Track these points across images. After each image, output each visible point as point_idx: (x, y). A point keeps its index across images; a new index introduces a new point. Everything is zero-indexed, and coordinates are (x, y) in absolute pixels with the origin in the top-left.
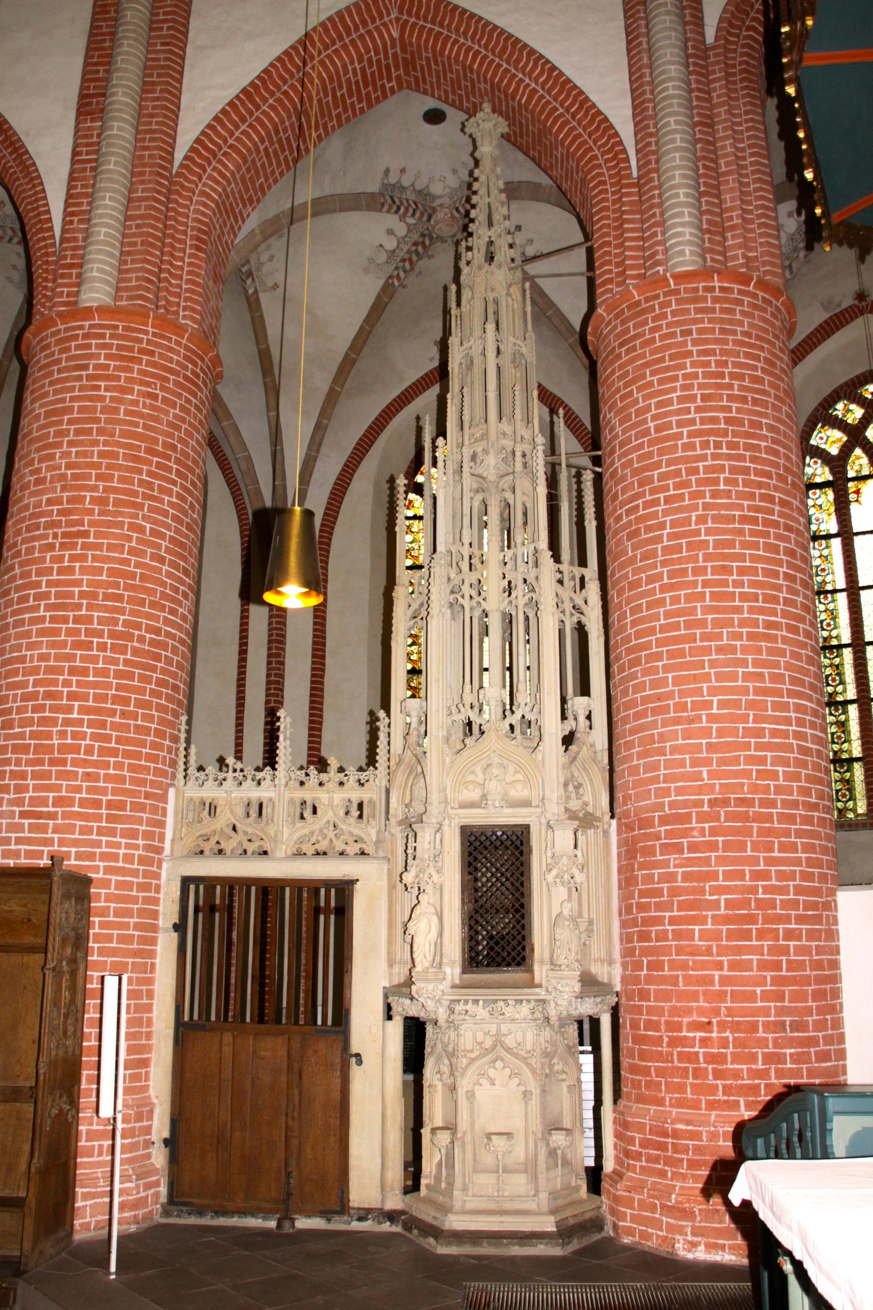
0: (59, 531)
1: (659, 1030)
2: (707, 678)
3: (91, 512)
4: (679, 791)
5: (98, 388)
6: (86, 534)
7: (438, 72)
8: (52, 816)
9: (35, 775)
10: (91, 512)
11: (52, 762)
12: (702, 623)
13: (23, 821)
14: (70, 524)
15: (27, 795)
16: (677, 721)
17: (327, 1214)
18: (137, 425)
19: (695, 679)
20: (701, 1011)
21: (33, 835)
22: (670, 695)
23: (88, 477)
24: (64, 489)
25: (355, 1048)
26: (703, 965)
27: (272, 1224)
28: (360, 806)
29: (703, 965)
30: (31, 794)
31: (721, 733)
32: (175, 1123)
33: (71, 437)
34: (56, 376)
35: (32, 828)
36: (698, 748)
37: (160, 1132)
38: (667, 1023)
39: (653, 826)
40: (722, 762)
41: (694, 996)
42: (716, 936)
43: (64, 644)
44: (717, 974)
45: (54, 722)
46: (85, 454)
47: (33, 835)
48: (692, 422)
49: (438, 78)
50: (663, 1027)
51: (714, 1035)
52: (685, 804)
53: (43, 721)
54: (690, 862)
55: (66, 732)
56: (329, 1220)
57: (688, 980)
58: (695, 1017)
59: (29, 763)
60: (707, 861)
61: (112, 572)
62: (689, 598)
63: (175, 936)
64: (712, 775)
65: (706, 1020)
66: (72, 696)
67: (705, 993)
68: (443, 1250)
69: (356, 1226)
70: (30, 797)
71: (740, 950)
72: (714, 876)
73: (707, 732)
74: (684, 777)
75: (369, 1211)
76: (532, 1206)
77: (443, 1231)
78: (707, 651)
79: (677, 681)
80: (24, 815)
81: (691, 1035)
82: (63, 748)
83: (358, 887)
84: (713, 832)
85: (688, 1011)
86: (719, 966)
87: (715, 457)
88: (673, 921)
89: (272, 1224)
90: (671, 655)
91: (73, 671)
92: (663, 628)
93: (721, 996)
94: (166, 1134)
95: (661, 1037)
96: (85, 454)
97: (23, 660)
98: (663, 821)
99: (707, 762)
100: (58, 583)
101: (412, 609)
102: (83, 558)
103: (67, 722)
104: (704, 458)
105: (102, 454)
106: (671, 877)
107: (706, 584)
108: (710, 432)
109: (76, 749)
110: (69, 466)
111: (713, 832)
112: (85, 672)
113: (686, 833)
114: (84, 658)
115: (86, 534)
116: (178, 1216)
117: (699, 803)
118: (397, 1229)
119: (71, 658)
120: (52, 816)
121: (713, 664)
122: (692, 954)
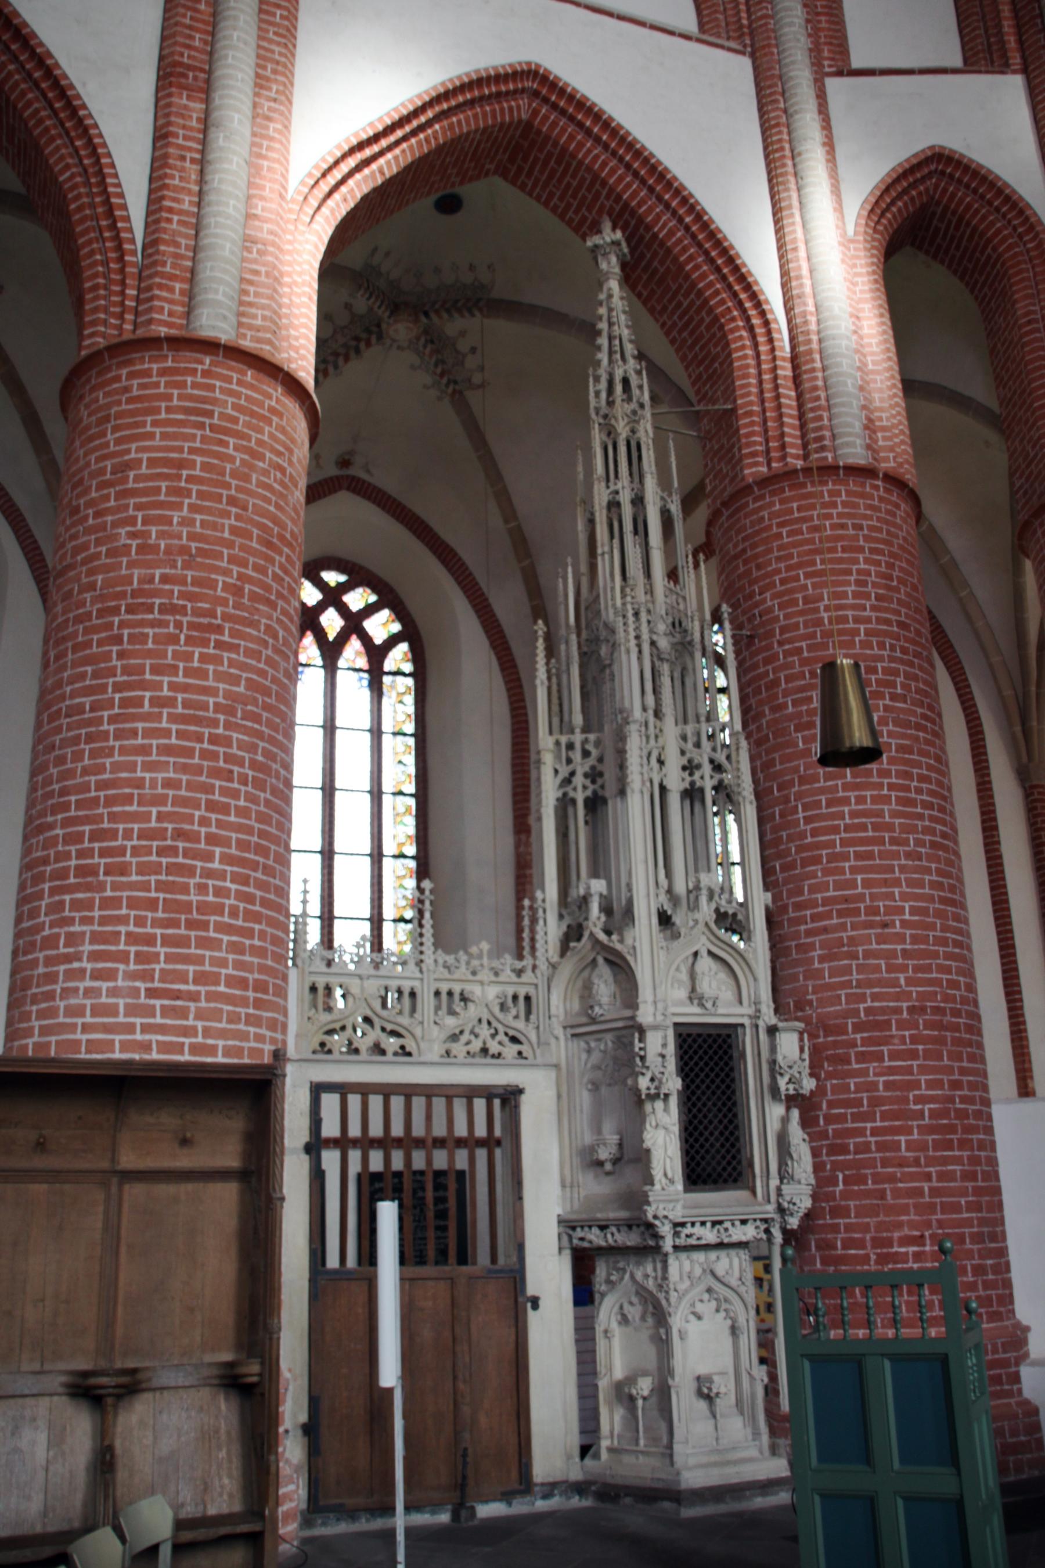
0: (185, 620)
1: (864, 1247)
2: (897, 883)
3: (224, 602)
4: (875, 997)
5: (225, 444)
6: (219, 629)
7: (553, 171)
8: (194, 997)
9: (167, 941)
10: (224, 602)
11: (191, 925)
12: (890, 828)
13: (152, 1002)
14: (196, 612)
15: (157, 967)
16: (870, 925)
17: (507, 1497)
18: (268, 501)
19: (885, 883)
20: (912, 1225)
21: (169, 1022)
22: (861, 898)
23: (219, 556)
24: (187, 566)
25: (531, 1290)
26: (912, 1177)
27: (444, 1518)
28: (528, 998)
29: (912, 1177)
30: (162, 965)
31: (915, 939)
32: (314, 1402)
33: (193, 500)
34: (163, 415)
35: (166, 1011)
36: (893, 954)
37: (294, 1415)
38: (873, 1239)
39: (846, 1033)
40: (917, 969)
41: (904, 1210)
42: (922, 1147)
43: (198, 770)
44: (926, 1186)
45: (191, 871)
46: (214, 526)
47: (169, 1022)
48: (868, 620)
49: (551, 177)
50: (869, 1244)
51: (928, 1248)
52: (883, 1010)
53: (174, 869)
54: (892, 1071)
55: (206, 886)
56: (510, 1504)
57: (897, 1193)
58: (906, 1231)
59: (156, 923)
60: (909, 1070)
61: (251, 684)
62: (875, 800)
63: (305, 1158)
64: (909, 981)
65: (917, 1233)
66: (211, 839)
67: (915, 1206)
68: (688, 1512)
69: (541, 1505)
70: (162, 970)
71: (945, 1161)
72: (916, 1085)
73: (901, 938)
74: (880, 983)
75: (553, 1485)
76: (753, 1453)
77: (679, 1492)
78: (896, 856)
79: (866, 884)
80: (151, 993)
81: (903, 1250)
82: (204, 908)
83: (524, 1099)
84: (914, 1040)
85: (899, 1225)
86: (928, 1177)
87: (892, 659)
88: (875, 1132)
89: (444, 1518)
90: (858, 856)
91: (211, 806)
92: (848, 828)
93: (931, 1208)
94: (303, 1417)
95: (867, 1256)
96: (214, 526)
97: (139, 784)
98: (858, 1028)
99: (903, 968)
100: (185, 688)
101: (560, 777)
102: (217, 660)
103: (209, 874)
104: (881, 658)
105: (234, 530)
106: (872, 1086)
107: (891, 787)
108: (887, 634)
109: (219, 909)
110: (192, 537)
111: (914, 1040)
112: (225, 809)
113: (886, 1041)
114: (224, 791)
115: (219, 629)
116: (324, 1524)
117: (898, 1011)
118: (587, 1503)
119: (208, 789)
120: (194, 997)
121: (903, 869)
122: (900, 1165)
